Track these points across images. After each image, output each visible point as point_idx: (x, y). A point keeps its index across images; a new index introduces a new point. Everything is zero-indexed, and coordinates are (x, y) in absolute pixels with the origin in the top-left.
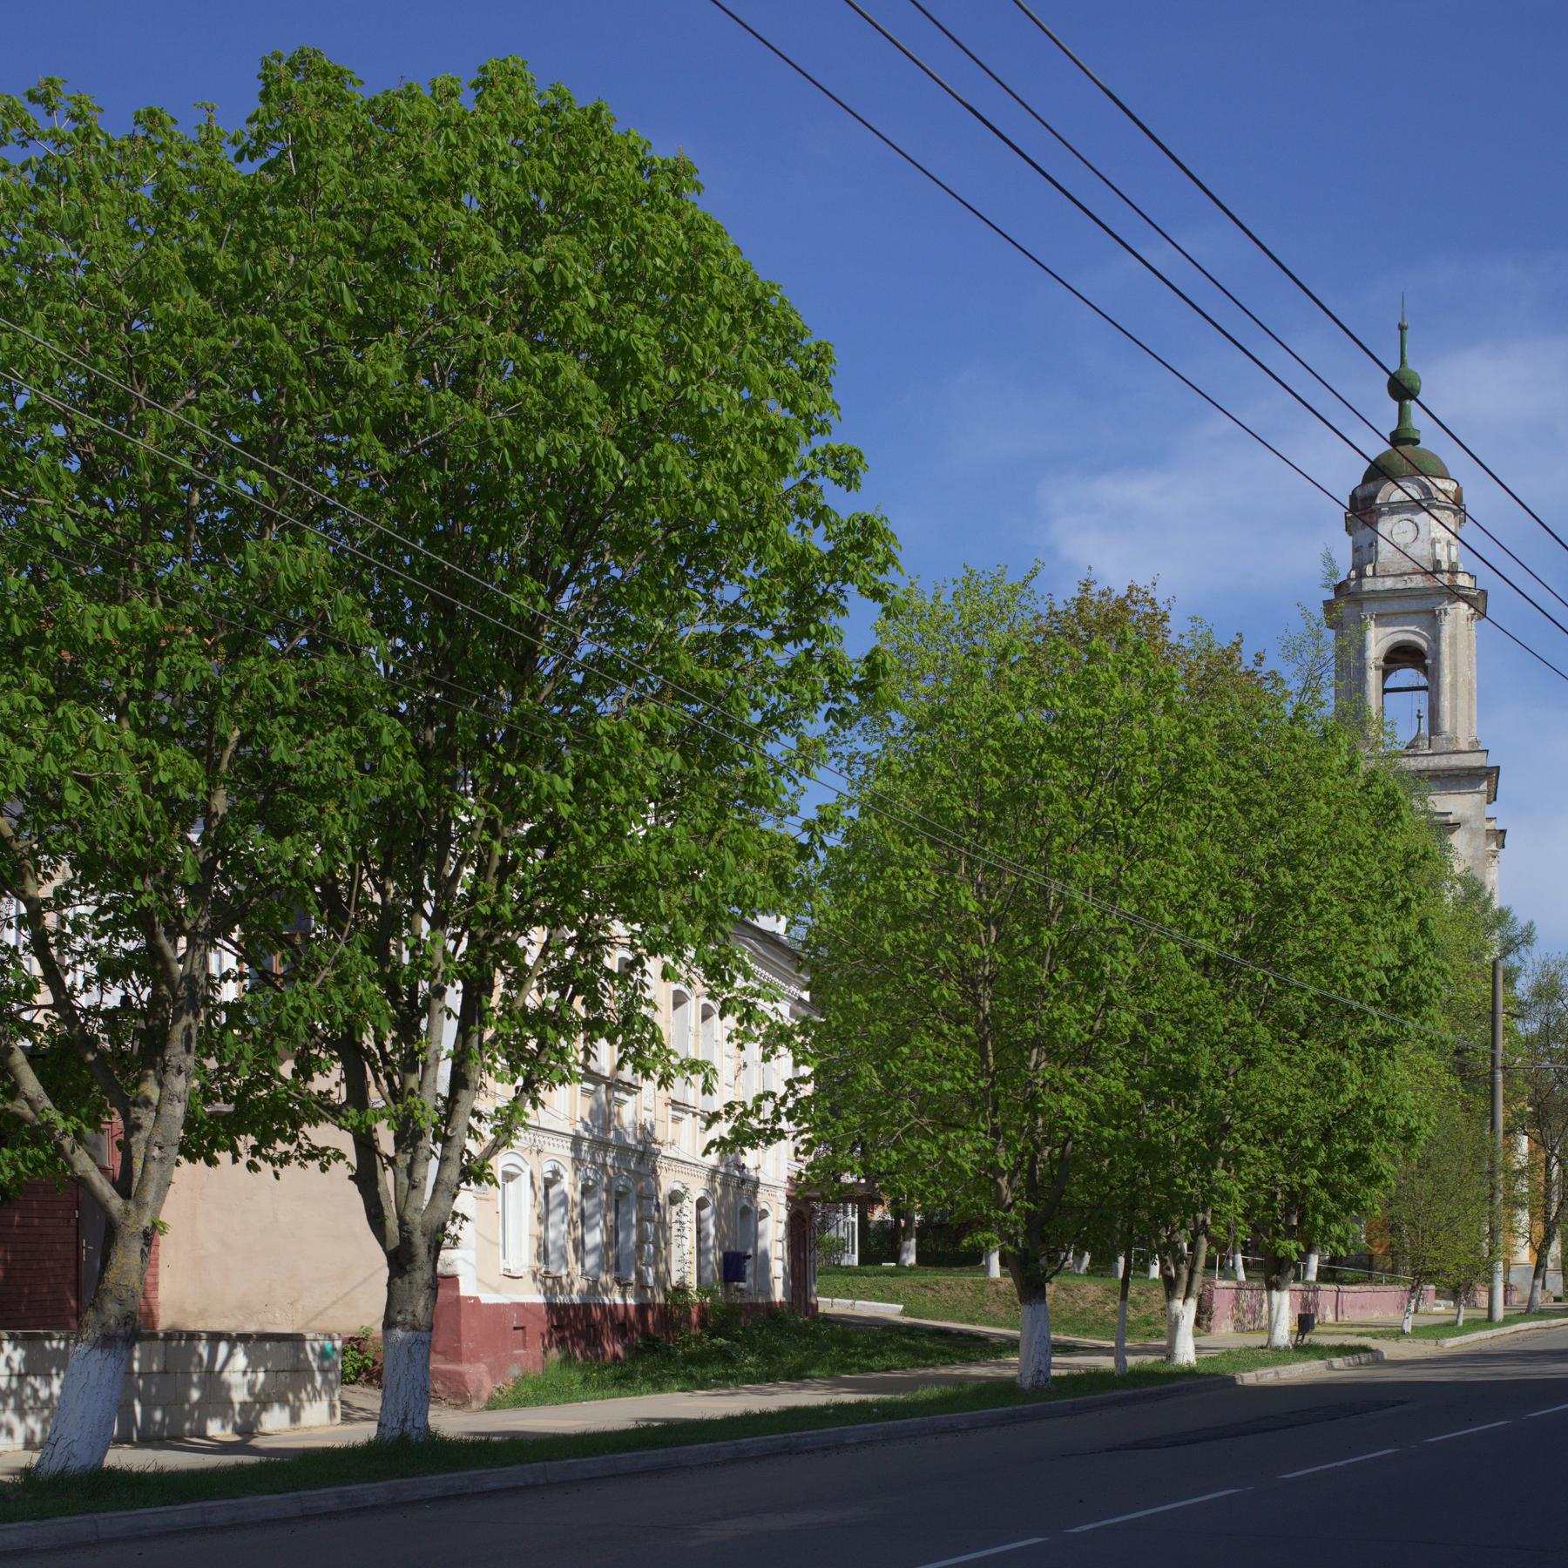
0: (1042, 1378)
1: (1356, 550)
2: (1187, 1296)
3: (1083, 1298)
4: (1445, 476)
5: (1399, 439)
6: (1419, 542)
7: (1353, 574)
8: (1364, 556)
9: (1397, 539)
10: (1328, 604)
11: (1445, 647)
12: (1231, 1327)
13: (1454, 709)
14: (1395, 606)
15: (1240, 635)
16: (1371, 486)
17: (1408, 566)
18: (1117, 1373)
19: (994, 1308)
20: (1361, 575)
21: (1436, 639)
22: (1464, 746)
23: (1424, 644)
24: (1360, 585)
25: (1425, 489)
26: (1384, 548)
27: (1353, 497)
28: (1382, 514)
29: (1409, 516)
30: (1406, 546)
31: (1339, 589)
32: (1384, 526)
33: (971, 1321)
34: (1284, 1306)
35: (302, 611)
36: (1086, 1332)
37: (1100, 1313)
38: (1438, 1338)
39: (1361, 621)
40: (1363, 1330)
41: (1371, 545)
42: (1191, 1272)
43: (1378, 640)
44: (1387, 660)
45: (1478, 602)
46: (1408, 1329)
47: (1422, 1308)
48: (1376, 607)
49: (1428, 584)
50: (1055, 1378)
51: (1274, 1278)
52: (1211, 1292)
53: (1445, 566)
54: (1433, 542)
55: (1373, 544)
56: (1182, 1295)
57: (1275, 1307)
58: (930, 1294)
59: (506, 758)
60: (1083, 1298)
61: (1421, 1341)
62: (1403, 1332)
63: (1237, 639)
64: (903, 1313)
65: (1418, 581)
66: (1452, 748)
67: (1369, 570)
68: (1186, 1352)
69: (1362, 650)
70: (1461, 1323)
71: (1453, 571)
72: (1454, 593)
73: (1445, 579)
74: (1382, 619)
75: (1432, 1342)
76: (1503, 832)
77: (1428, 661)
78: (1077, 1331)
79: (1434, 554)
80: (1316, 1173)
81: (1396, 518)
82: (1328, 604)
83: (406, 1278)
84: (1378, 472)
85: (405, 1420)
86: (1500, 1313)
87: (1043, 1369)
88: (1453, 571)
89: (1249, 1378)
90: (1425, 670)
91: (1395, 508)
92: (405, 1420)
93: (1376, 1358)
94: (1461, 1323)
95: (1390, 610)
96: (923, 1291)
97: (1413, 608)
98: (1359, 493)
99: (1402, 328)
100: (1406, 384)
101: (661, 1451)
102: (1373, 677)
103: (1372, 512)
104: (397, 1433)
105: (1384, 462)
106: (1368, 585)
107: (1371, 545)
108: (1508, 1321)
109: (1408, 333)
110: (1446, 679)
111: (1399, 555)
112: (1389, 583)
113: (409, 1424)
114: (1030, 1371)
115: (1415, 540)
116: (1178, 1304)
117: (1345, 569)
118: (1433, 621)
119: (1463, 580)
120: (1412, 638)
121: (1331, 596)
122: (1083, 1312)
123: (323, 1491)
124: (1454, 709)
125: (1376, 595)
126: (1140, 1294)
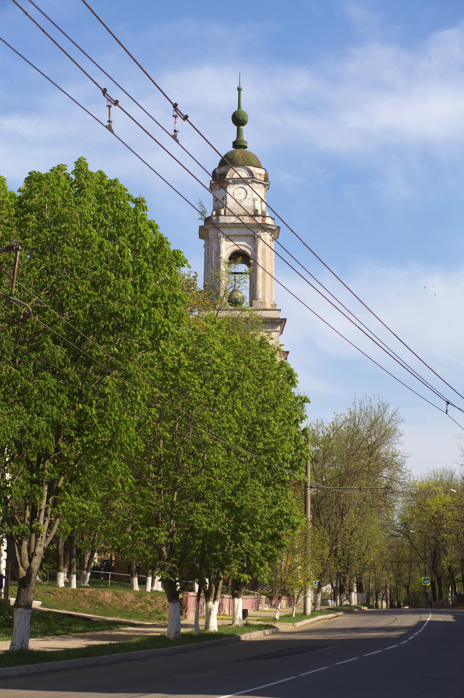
0: (178, 635)
1: (216, 200)
2: (215, 600)
3: (126, 600)
4: (260, 167)
5: (238, 145)
6: (247, 199)
7: (214, 212)
8: (220, 203)
9: (236, 197)
10: (201, 227)
11: (260, 255)
12: (221, 614)
13: (264, 287)
14: (235, 231)
15: (195, 273)
16: (223, 169)
17: (241, 211)
18: (195, 634)
19: (84, 604)
20: (218, 214)
21: (255, 250)
22: (268, 307)
23: (249, 252)
24: (218, 219)
25: (250, 173)
26: (230, 202)
27: (214, 172)
28: (229, 184)
29: (242, 185)
30: (241, 201)
31: (207, 220)
32: (231, 189)
33: (75, 610)
34: (240, 603)
35: (363, 503)
36: (130, 617)
37: (135, 607)
38: (293, 622)
39: (219, 239)
40: (259, 618)
41: (223, 199)
42: (217, 589)
43: (227, 248)
44: (230, 258)
45: (275, 232)
46: (277, 618)
47: (260, 608)
48: (226, 231)
49: (252, 221)
50: (182, 634)
51: (236, 592)
52: (187, 598)
53: (260, 213)
54: (254, 200)
55: (224, 198)
56: (212, 599)
57: (236, 605)
58: (52, 596)
59: (79, 403)
60: (126, 600)
61: (286, 624)
62: (275, 619)
63: (194, 275)
64: (42, 605)
65: (247, 220)
66: (263, 307)
67: (222, 212)
68: (214, 626)
69: (218, 252)
70: (294, 615)
71: (264, 216)
72: (264, 227)
73: (259, 220)
74: (228, 238)
75: (291, 624)
76: (288, 352)
77: (251, 261)
78: (125, 616)
79: (254, 206)
80: (259, 544)
81: (236, 186)
82: (201, 227)
83: (26, 589)
84: (227, 162)
85: (22, 643)
86: (309, 611)
87: (178, 632)
88: (264, 216)
89: (245, 637)
90: (249, 265)
91: (235, 181)
92: (22, 643)
93: (277, 632)
94: (294, 615)
95: (233, 233)
96: (48, 594)
97: (245, 233)
98: (217, 171)
99: (239, 90)
100: (241, 118)
101: (94, 658)
102: (223, 268)
103: (224, 182)
104: (19, 648)
105: (230, 157)
106: (222, 220)
107: (223, 199)
108: (314, 613)
109: (242, 92)
110: (260, 271)
111: (237, 205)
112: (232, 220)
113: (24, 644)
114: (173, 632)
115: (243, 198)
116: (211, 603)
117: (209, 212)
118: (254, 239)
119: (269, 221)
120: (243, 248)
121: (202, 223)
122: (127, 607)
123: (23, 666)
124: (264, 287)
125: (226, 225)
126: (152, 598)
